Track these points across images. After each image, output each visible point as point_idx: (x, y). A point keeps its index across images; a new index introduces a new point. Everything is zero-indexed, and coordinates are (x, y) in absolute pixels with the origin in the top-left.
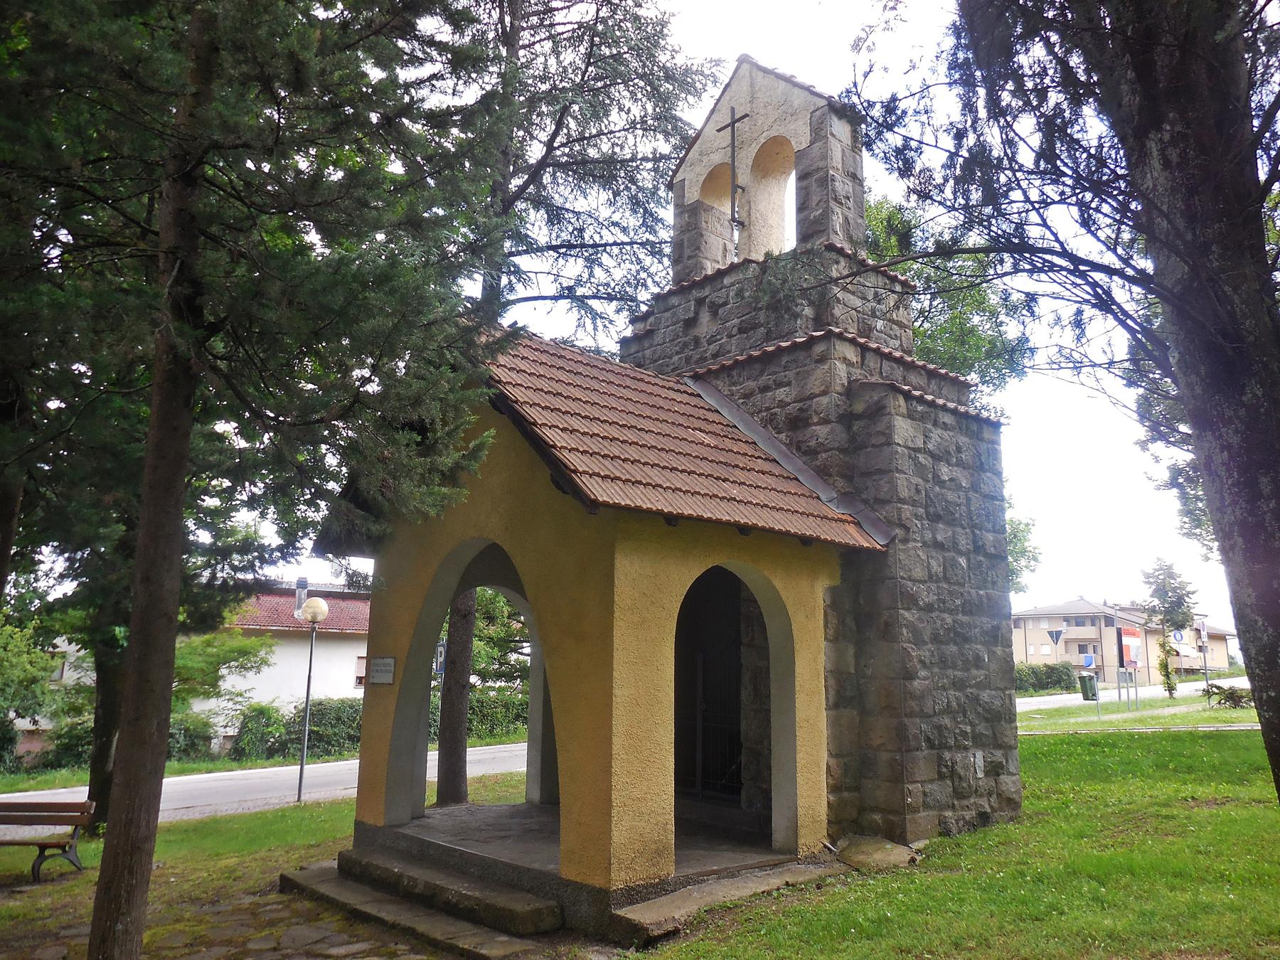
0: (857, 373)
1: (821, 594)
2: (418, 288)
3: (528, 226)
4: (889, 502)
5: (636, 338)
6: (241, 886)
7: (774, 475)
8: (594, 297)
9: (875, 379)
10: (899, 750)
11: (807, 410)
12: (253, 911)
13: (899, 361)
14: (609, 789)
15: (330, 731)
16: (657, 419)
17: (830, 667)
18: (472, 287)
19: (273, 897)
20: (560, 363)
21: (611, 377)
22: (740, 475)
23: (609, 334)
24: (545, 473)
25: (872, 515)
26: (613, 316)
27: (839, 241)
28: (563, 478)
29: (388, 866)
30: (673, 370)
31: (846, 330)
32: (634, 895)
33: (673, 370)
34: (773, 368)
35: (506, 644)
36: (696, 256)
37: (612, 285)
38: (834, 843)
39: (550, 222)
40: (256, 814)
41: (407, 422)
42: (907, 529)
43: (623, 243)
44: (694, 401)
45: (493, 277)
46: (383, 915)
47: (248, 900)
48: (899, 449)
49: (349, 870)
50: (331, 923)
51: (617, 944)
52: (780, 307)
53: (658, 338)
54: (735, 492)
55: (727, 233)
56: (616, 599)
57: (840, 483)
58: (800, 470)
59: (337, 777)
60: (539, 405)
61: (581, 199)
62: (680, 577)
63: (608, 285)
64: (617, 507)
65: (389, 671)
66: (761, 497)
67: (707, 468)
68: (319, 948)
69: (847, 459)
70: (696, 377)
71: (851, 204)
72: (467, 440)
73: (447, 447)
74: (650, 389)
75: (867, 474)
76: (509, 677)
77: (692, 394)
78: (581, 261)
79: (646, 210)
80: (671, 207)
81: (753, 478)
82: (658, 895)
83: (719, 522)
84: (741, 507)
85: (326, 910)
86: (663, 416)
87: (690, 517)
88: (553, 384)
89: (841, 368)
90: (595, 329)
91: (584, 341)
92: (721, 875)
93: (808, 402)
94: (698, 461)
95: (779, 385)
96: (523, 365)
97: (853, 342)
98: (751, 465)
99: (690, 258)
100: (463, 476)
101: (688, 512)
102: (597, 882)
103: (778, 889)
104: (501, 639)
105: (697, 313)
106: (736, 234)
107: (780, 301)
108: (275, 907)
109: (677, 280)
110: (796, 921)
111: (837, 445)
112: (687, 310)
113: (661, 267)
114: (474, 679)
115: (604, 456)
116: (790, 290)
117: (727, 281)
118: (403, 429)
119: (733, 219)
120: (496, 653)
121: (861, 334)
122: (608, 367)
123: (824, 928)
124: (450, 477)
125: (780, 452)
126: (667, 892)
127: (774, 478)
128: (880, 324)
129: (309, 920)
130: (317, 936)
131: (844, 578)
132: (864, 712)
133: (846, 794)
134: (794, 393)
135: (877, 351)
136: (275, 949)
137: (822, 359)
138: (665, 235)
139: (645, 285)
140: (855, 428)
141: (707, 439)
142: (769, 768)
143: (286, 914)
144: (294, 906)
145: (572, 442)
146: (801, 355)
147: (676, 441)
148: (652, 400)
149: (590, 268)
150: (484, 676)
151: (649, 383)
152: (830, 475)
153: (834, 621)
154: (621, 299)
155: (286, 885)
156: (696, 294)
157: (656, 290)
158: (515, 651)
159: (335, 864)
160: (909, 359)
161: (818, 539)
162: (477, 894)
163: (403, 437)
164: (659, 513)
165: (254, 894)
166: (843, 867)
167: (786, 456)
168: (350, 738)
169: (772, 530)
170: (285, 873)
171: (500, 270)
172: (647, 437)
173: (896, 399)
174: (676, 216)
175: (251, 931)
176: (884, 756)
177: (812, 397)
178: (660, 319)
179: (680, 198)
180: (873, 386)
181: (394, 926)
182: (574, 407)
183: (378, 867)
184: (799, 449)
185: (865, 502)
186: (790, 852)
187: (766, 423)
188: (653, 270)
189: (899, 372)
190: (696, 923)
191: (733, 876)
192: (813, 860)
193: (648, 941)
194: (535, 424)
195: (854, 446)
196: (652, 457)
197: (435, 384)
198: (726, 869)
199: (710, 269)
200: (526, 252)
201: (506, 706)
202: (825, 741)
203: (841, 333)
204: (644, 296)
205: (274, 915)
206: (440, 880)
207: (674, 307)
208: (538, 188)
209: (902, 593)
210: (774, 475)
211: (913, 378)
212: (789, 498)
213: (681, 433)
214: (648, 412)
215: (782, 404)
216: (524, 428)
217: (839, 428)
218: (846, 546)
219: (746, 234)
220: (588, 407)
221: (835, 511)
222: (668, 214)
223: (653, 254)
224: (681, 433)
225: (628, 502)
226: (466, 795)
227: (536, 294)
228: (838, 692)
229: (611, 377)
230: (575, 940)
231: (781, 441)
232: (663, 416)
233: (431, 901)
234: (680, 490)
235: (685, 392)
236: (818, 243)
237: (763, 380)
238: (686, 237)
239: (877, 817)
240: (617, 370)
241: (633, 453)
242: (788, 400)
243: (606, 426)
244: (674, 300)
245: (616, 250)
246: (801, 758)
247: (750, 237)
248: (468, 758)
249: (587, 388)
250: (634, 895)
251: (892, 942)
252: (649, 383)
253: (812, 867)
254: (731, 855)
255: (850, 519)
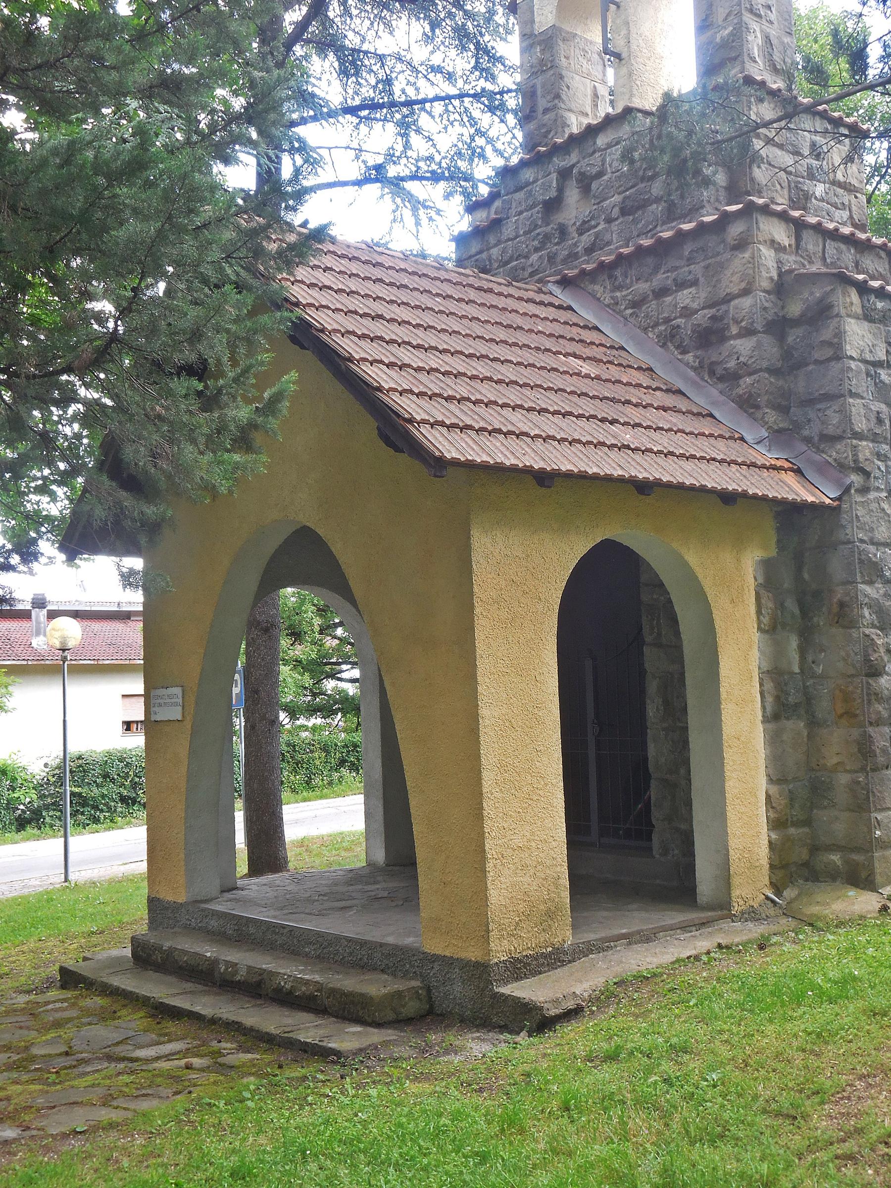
0: (791, 261)
1: (750, 571)
2: (185, 176)
3: (312, 80)
4: (839, 438)
5: (478, 232)
6: (10, 983)
7: (679, 411)
8: (414, 177)
9: (816, 268)
10: (863, 769)
11: (722, 318)
12: (31, 1011)
13: (850, 240)
14: (481, 836)
15: (96, 791)
16: (515, 344)
17: (766, 666)
18: (240, 175)
19: (53, 994)
20: (377, 273)
21: (449, 290)
22: (636, 415)
23: (437, 230)
24: (369, 426)
25: (817, 457)
26: (441, 204)
27: (759, 71)
28: (395, 432)
29: (198, 950)
30: (532, 275)
31: (773, 201)
32: (521, 968)
33: (532, 275)
34: (672, 262)
35: (320, 668)
36: (555, 107)
37: (437, 158)
38: (778, 892)
39: (344, 72)
40: (14, 899)
41: (171, 363)
42: (867, 474)
43: (449, 98)
44: (564, 316)
45: (269, 158)
46: (197, 1009)
47: (22, 999)
48: (853, 365)
49: (144, 957)
50: (133, 1021)
51: (503, 1028)
52: (685, 171)
53: (508, 231)
54: (628, 436)
55: (596, 72)
56: (476, 589)
57: (772, 416)
58: (714, 403)
59: (116, 851)
60: (353, 333)
61: (385, 36)
62: (558, 557)
63: (430, 158)
64: (470, 465)
65: (176, 704)
66: (663, 442)
67: (587, 407)
68: (120, 1050)
69: (781, 383)
70: (565, 282)
71: (773, 16)
72: (260, 388)
73: (234, 398)
74: (501, 302)
75: (810, 402)
76: (327, 711)
77: (560, 307)
78: (390, 127)
79: (478, 45)
80: (515, 39)
81: (652, 417)
82: (552, 967)
83: (608, 479)
84: (638, 457)
85: (125, 1006)
86: (523, 338)
87: (569, 475)
88: (370, 302)
89: (768, 256)
90: (418, 224)
91: (402, 241)
92: (631, 939)
93: (724, 307)
94: (575, 398)
95: (682, 285)
96: (326, 279)
97: (783, 216)
98: (647, 399)
99: (546, 111)
100: (258, 438)
101: (565, 467)
102: (473, 954)
103: (708, 953)
104: (312, 662)
105: (561, 190)
106: (610, 72)
107: (685, 161)
108: (58, 1005)
109: (530, 145)
110: (736, 987)
111: (765, 364)
112: (546, 187)
113: (503, 128)
114: (283, 716)
115: (449, 399)
116: (699, 144)
117: (601, 141)
118: (178, 375)
119: (606, 51)
120: (307, 681)
121: (794, 205)
122: (443, 275)
123: (772, 994)
124: (244, 440)
125: (686, 379)
126: (563, 963)
127: (680, 416)
128: (820, 189)
129: (104, 1019)
130: (117, 1036)
131: (781, 545)
132: (813, 723)
133: (792, 831)
134: (703, 295)
135: (818, 228)
136: (67, 1054)
137: (741, 245)
138: (506, 80)
139: (482, 156)
140: (790, 339)
141: (586, 368)
142: (689, 804)
143: (73, 1013)
144: (82, 1003)
145: (403, 380)
146: (711, 241)
147: (544, 373)
148: (506, 318)
149: (405, 135)
150: (293, 714)
151: (500, 294)
152: (757, 407)
153: (769, 604)
154: (451, 178)
155: (69, 979)
156: (559, 162)
157: (499, 162)
158: (332, 676)
159: (128, 952)
160: (863, 236)
161: (744, 495)
162: (317, 978)
163: (181, 385)
164: (528, 471)
165: (29, 992)
166: (793, 923)
167: (694, 384)
168: (123, 799)
169: (681, 487)
170: (65, 965)
171: (278, 148)
172: (503, 368)
173: (845, 294)
174: (523, 51)
175: (34, 1034)
176: (843, 779)
177: (728, 299)
178: (510, 202)
179: (528, 23)
180: (815, 278)
181: (213, 1021)
182: (402, 333)
183: (185, 952)
184: (712, 373)
185: (808, 440)
186: (722, 908)
187: (665, 341)
188: (492, 133)
189: (849, 256)
190: (603, 999)
191: (648, 940)
192: (752, 915)
193: (542, 1023)
194: (350, 359)
195: (791, 364)
196: (512, 396)
197: (218, 310)
198: (638, 932)
199: (575, 124)
200: (314, 119)
201: (325, 749)
202: (763, 769)
203: (766, 206)
204: (483, 171)
205: (58, 1015)
206: (265, 962)
207: (528, 184)
208: (323, 24)
209: (861, 561)
210: (679, 411)
211: (870, 263)
212: (703, 442)
213: (549, 361)
214: (502, 334)
215: (687, 312)
216: (337, 365)
217: (767, 340)
218: (783, 502)
219: (624, 71)
220: (420, 332)
221: (767, 456)
222: (510, 49)
223: (492, 109)
224: (549, 361)
225: (485, 458)
226: (286, 862)
227: (332, 179)
228: (777, 698)
229: (449, 290)
230: (448, 1027)
231: (687, 364)
232: (523, 338)
233: (257, 989)
234: (553, 438)
235: (551, 304)
236: (734, 73)
237: (660, 279)
238: (539, 81)
239: (835, 858)
240: (455, 278)
241: (487, 392)
242: (695, 305)
243: (447, 358)
244: (528, 174)
245: (438, 107)
246: (732, 786)
247: (630, 74)
248: (286, 817)
249: (417, 307)
250: (521, 968)
251: (860, 1004)
252: (500, 294)
253: (750, 925)
254: (644, 914)
255: (787, 465)
